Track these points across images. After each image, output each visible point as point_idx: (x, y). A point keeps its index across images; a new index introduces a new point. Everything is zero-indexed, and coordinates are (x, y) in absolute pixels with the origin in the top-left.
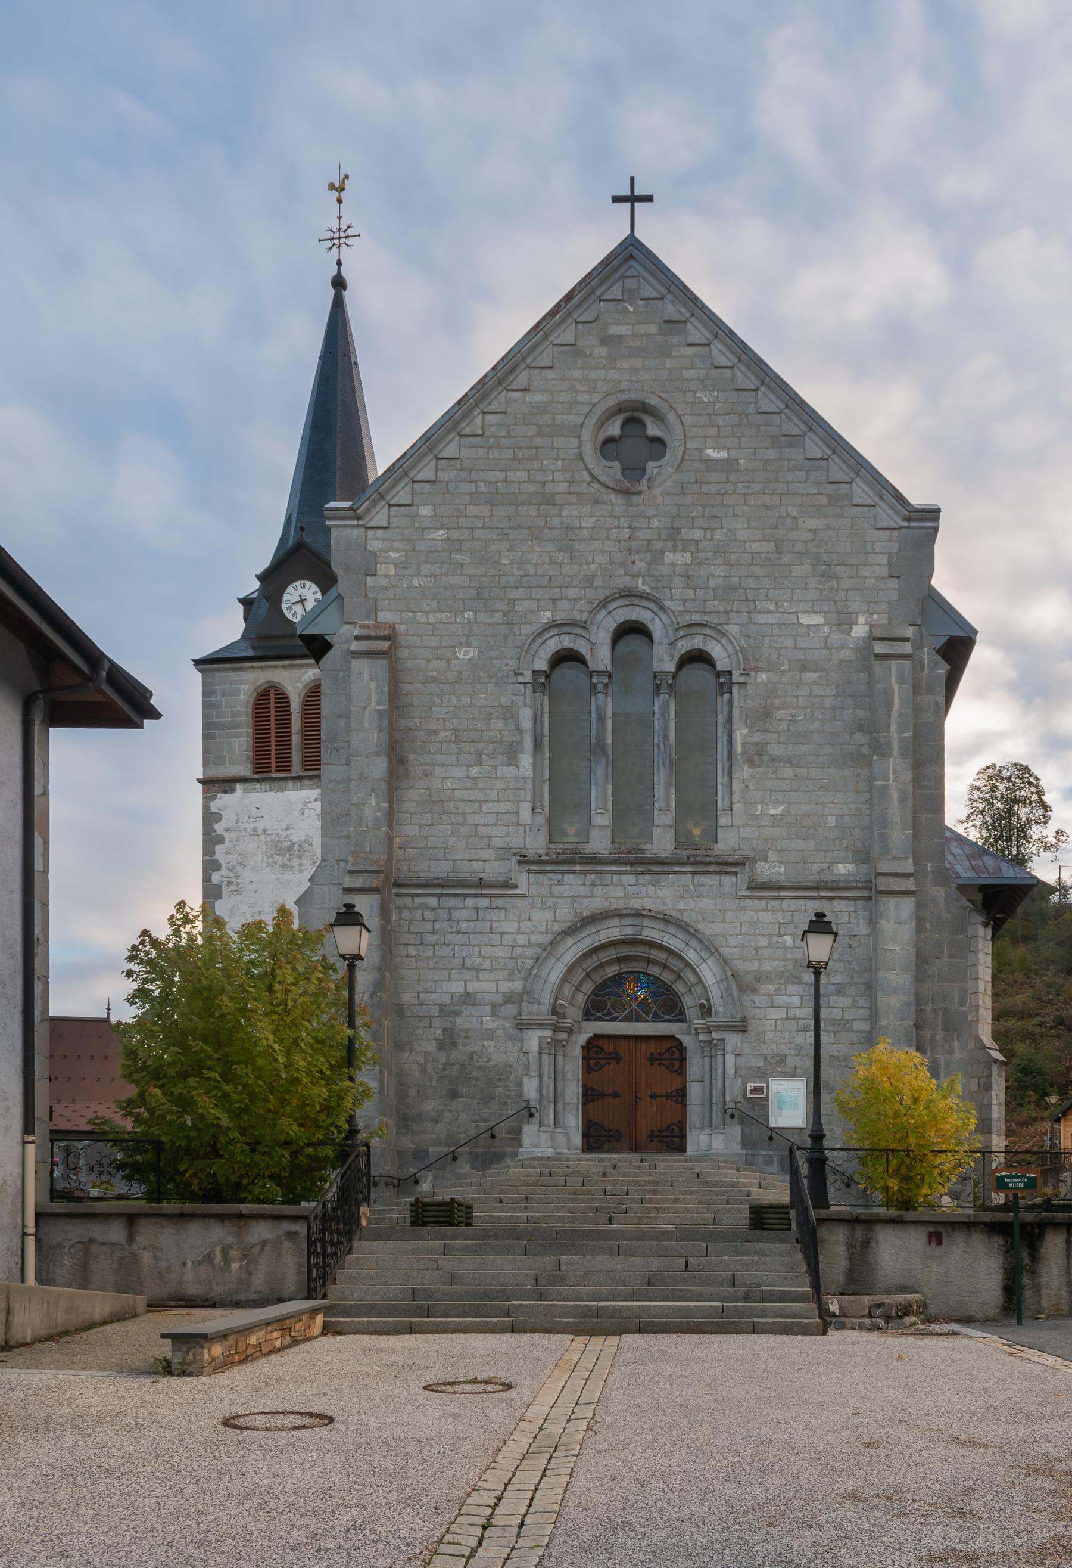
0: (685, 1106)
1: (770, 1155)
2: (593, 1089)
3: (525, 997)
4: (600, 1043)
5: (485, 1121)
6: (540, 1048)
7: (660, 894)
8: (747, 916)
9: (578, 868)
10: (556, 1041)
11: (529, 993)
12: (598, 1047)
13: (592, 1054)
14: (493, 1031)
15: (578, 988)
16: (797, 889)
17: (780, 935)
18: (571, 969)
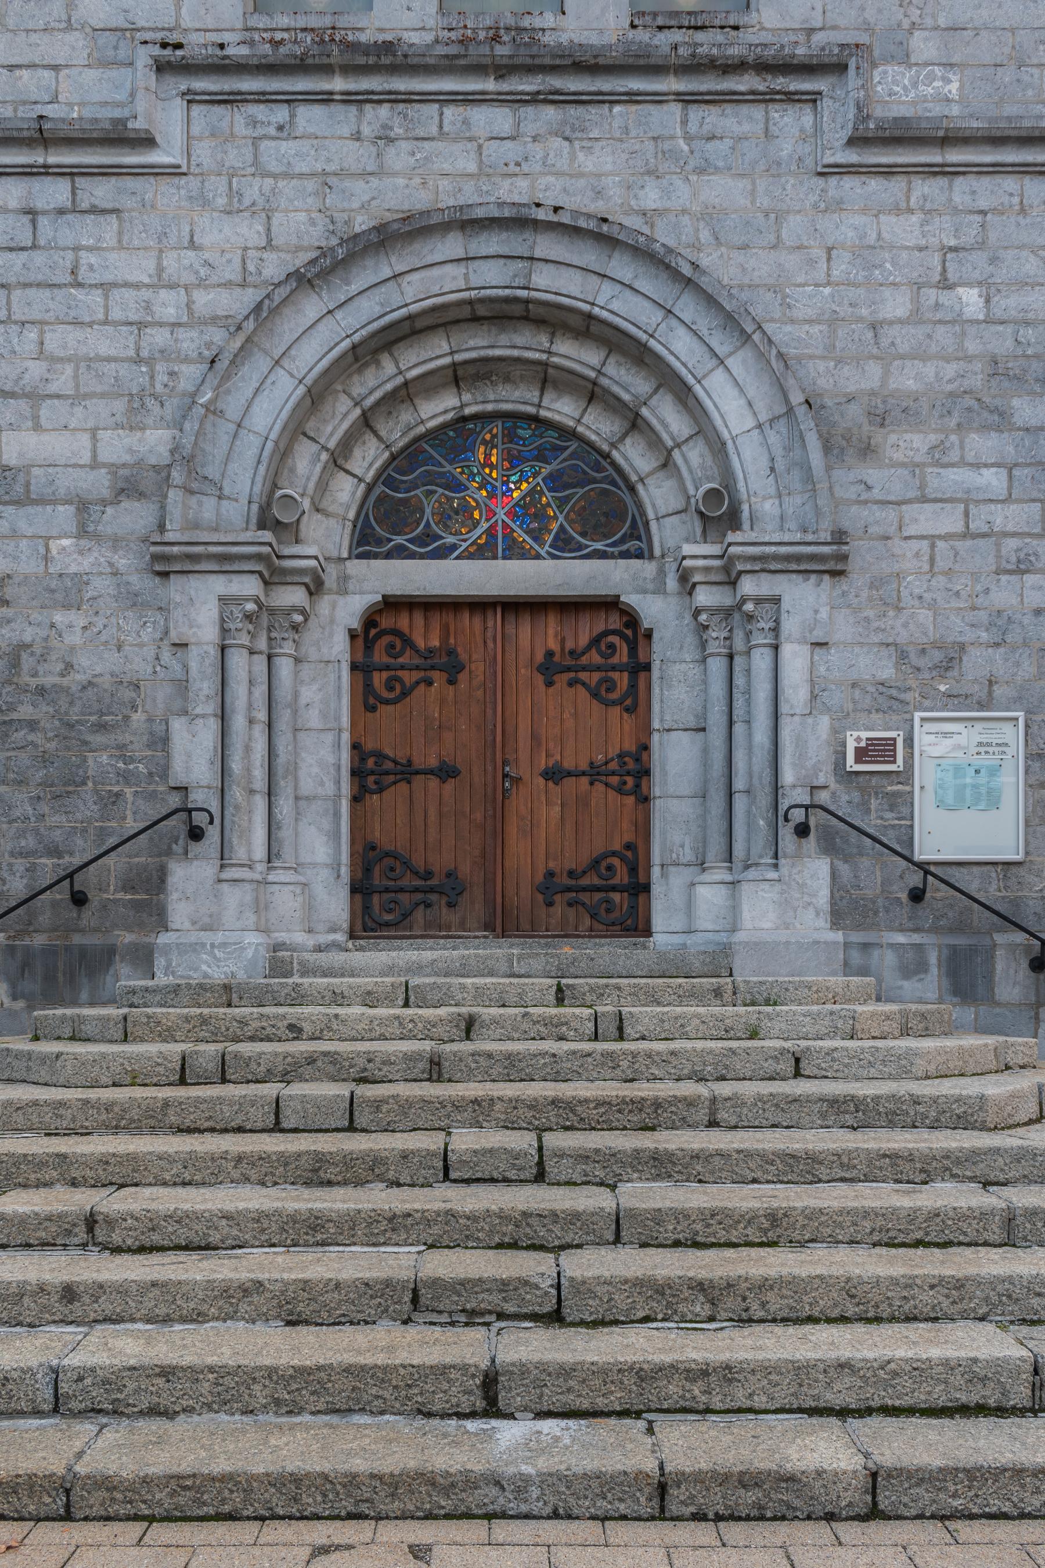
0: (646, 800)
1: (919, 947)
2: (379, 755)
3: (177, 476)
4: (403, 622)
5: (55, 852)
6: (224, 631)
7: (588, 163)
8: (847, 228)
9: (338, 84)
10: (272, 611)
11: (189, 460)
12: (396, 632)
13: (379, 656)
14: (81, 581)
15: (337, 460)
16: (997, 140)
17: (945, 284)
18: (316, 396)
